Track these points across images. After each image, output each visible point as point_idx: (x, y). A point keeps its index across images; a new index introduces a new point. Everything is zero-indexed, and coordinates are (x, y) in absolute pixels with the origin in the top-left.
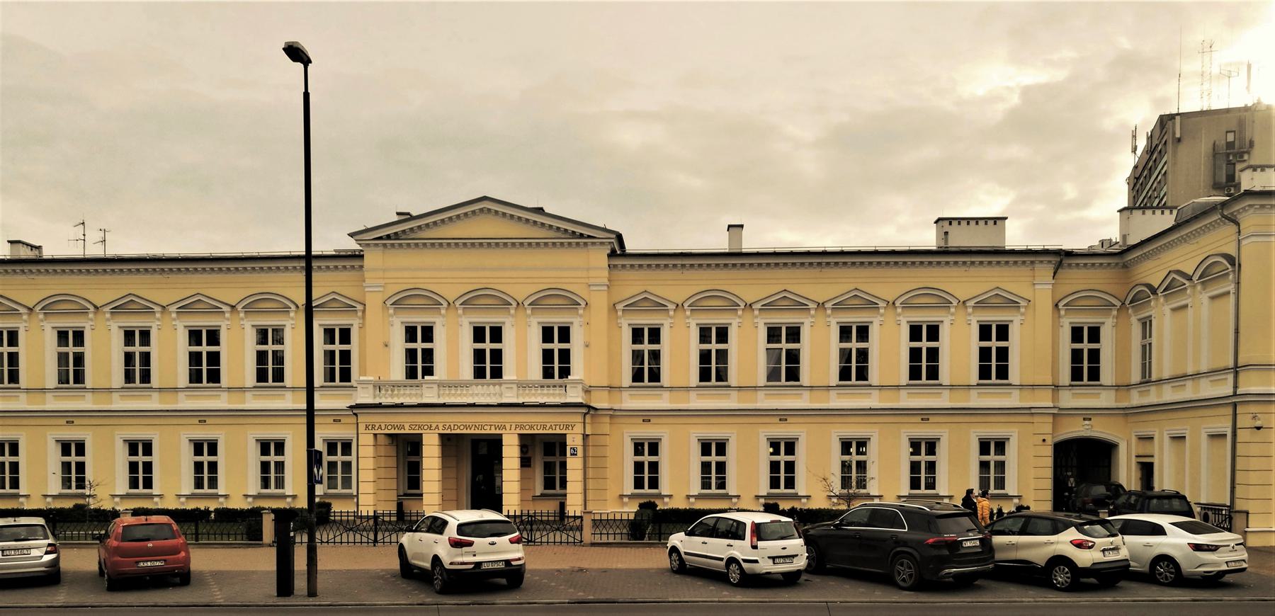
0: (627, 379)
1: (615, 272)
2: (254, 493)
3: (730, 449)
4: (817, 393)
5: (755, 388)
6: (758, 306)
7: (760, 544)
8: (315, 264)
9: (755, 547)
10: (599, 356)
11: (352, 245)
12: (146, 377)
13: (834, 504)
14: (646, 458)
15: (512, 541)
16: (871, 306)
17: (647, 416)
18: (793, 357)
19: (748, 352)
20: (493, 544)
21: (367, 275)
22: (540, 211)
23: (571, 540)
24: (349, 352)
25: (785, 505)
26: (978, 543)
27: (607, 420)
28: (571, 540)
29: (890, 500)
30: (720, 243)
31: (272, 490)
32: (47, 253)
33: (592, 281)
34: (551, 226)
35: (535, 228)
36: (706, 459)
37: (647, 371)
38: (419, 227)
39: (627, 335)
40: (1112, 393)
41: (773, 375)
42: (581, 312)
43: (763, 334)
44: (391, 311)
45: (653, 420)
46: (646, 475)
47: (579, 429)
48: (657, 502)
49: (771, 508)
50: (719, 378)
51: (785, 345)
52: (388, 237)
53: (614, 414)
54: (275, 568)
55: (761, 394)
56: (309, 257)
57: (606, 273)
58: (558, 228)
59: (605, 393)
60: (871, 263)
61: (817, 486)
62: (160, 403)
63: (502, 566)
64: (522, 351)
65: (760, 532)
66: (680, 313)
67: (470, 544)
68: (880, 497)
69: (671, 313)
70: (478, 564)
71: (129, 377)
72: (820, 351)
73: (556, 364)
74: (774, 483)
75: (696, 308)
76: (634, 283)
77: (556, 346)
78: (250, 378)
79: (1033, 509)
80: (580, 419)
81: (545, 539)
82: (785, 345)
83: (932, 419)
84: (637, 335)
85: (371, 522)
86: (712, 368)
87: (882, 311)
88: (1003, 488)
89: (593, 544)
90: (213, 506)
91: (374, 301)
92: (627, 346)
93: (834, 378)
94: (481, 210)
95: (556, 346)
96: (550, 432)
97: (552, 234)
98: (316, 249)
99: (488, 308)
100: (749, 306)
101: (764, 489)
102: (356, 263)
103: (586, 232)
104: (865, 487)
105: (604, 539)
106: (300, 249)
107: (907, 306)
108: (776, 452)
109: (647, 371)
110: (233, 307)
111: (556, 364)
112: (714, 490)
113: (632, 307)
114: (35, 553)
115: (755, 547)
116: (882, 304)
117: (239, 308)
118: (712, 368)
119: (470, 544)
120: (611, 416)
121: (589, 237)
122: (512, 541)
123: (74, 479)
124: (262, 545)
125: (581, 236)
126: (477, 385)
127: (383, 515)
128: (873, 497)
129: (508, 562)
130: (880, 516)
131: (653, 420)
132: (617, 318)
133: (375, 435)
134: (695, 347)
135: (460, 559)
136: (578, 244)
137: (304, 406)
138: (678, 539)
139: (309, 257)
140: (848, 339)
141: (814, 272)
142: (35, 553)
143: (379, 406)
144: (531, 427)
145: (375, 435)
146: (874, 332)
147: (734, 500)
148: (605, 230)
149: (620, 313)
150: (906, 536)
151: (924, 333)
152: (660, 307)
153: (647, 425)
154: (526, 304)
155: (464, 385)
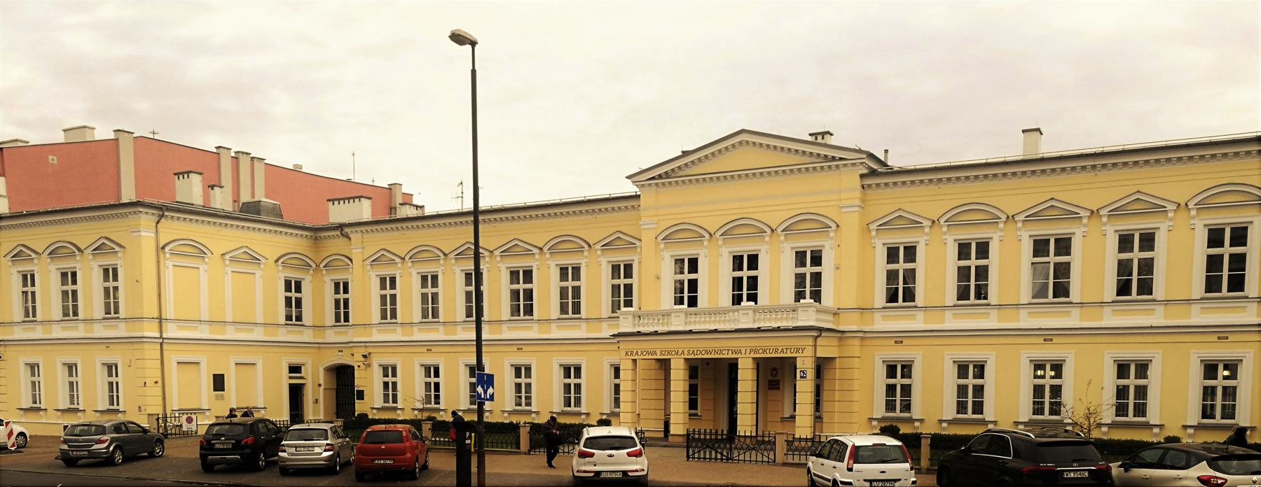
0: (880, 298)
1: (869, 192)
2: (558, 410)
3: (1153, 371)
4: (1173, 309)
5: (1102, 304)
6: (1022, 217)
7: (856, 466)
8: (480, 218)
9: (850, 470)
10: (852, 277)
11: (630, 189)
12: (577, 309)
13: (1104, 433)
14: (899, 381)
15: (629, 455)
16: (1071, 216)
17: (899, 338)
18: (1063, 271)
19: (1012, 267)
20: (611, 456)
21: (642, 213)
22: (685, 154)
23: (765, 459)
24: (579, 287)
25: (905, 429)
26: (1087, 474)
27: (857, 342)
28: (765, 459)
29: (1006, 425)
30: (1015, 151)
31: (573, 409)
32: (428, 211)
33: (845, 203)
34: (804, 152)
35: (783, 154)
36: (892, 381)
37: (900, 291)
38: (686, 165)
39: (882, 254)
40: (310, 331)
41: (1040, 292)
42: (832, 234)
43: (1027, 247)
44: (662, 246)
45: (906, 342)
46: (970, 400)
47: (809, 352)
48: (900, 426)
49: (885, 431)
50: (978, 297)
51: (1052, 259)
52: (660, 176)
53: (865, 336)
54: (454, 468)
55: (1195, 308)
56: (476, 212)
57: (858, 193)
58: (811, 154)
59: (855, 316)
60: (913, 182)
61: (934, 407)
62: (446, 334)
63: (619, 475)
64: (777, 277)
65: (859, 455)
66: (1095, 221)
67: (592, 455)
68: (995, 423)
69: (927, 230)
70: (598, 473)
71: (564, 309)
72: (1095, 263)
73: (809, 286)
74: (890, 406)
75: (952, 223)
76: (888, 201)
77: (745, 273)
78: (555, 312)
79: (1184, 441)
80: (811, 342)
81: (741, 457)
82: (1052, 259)
83: (1232, 338)
84: (892, 255)
85: (810, 444)
86: (972, 286)
87: (1171, 215)
88: (1144, 415)
89: (785, 464)
90: (979, 430)
91: (647, 237)
92: (881, 266)
93: (1110, 292)
94: (740, 143)
95: (809, 270)
96: (782, 355)
97: (806, 159)
98: (483, 205)
99: (747, 236)
100: (1011, 218)
101: (880, 411)
102: (634, 203)
103: (838, 154)
104: (1144, 415)
105: (796, 460)
106: (469, 206)
107: (1203, 207)
108: (386, 375)
109: (900, 291)
110: (491, 252)
111: (809, 286)
112: (970, 415)
113: (885, 226)
114: (317, 450)
115: (850, 470)
116: (1170, 207)
117: (545, 249)
118: (972, 286)
119: (592, 455)
120: (840, 338)
121: (841, 159)
122: (629, 455)
123: (898, 403)
124: (519, 453)
125: (834, 158)
126: (734, 311)
127: (800, 439)
128: (1151, 426)
129: (625, 473)
130: (996, 441)
131: (906, 342)
132: (871, 238)
133: (635, 361)
134: (1112, 255)
135: (584, 468)
136: (830, 167)
137: (474, 337)
138: (813, 463)
139: (476, 212)
140: (1220, 244)
141: (1087, 176)
142: (317, 450)
143: (639, 334)
144: (764, 351)
145: (635, 361)
146: (1161, 240)
147: (917, 424)
148: (860, 151)
149: (874, 233)
150: (1010, 465)
151: (974, 251)
152: (915, 224)
153: (899, 347)
154: (779, 230)
155: (723, 312)
